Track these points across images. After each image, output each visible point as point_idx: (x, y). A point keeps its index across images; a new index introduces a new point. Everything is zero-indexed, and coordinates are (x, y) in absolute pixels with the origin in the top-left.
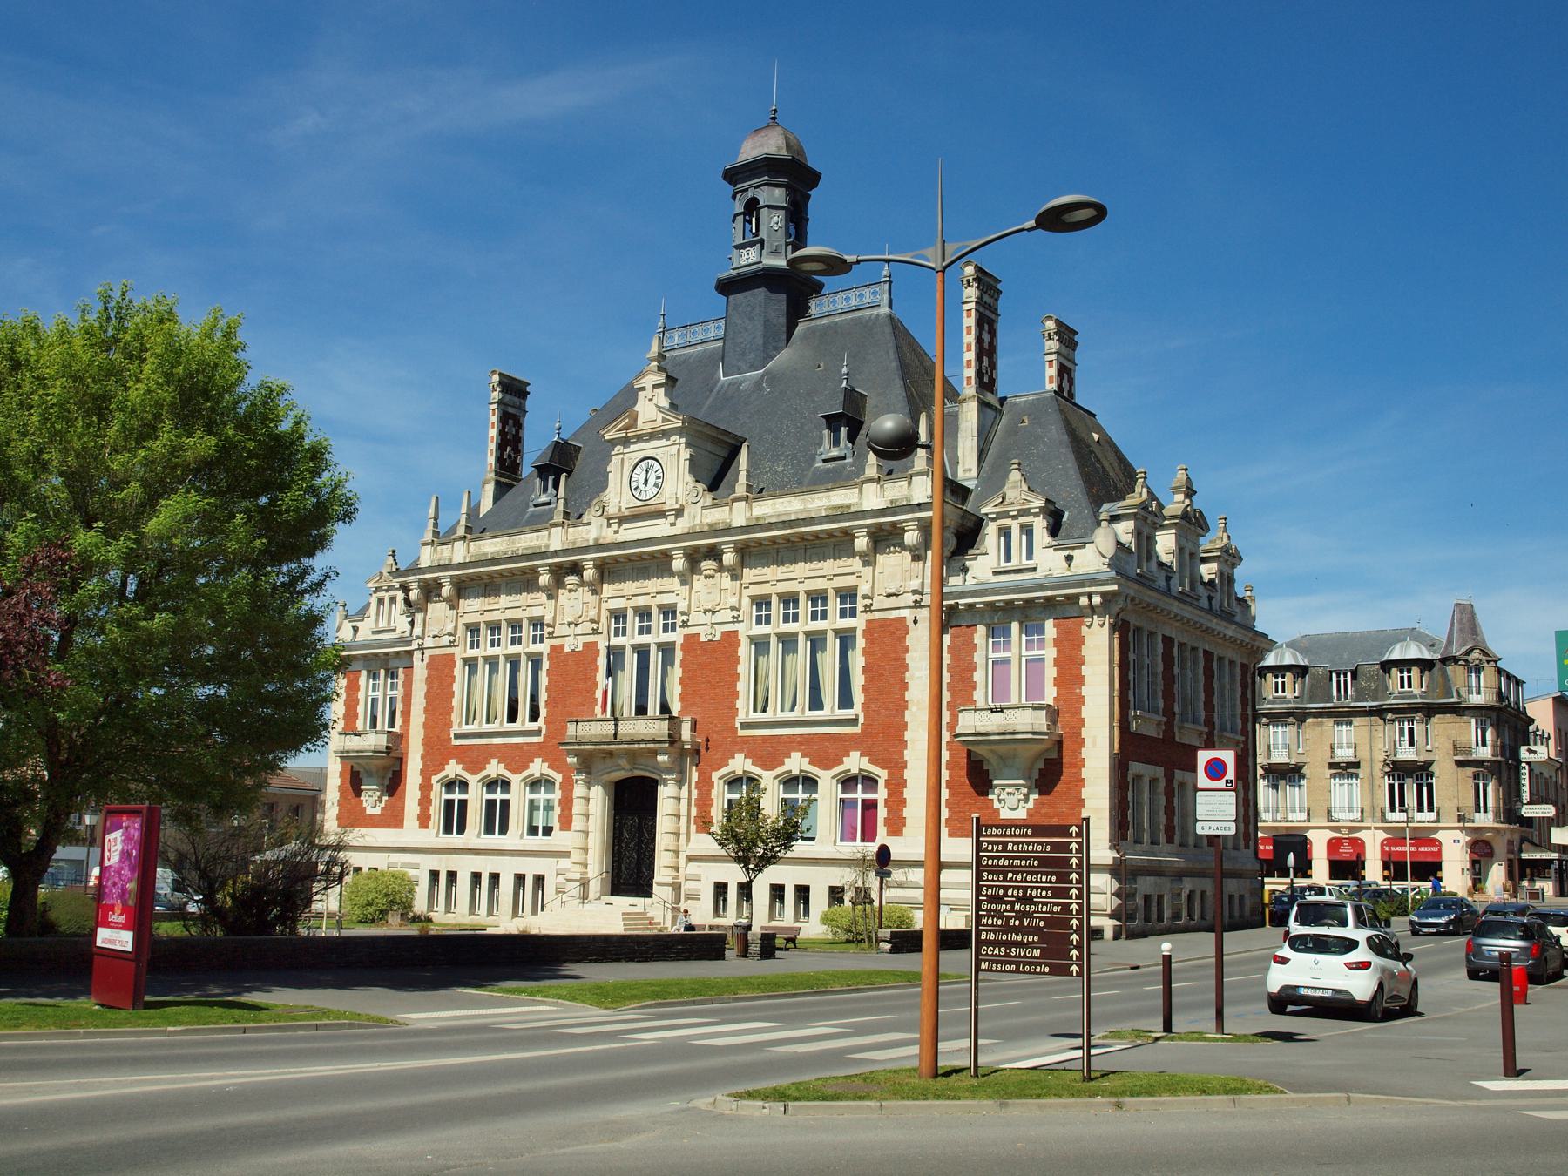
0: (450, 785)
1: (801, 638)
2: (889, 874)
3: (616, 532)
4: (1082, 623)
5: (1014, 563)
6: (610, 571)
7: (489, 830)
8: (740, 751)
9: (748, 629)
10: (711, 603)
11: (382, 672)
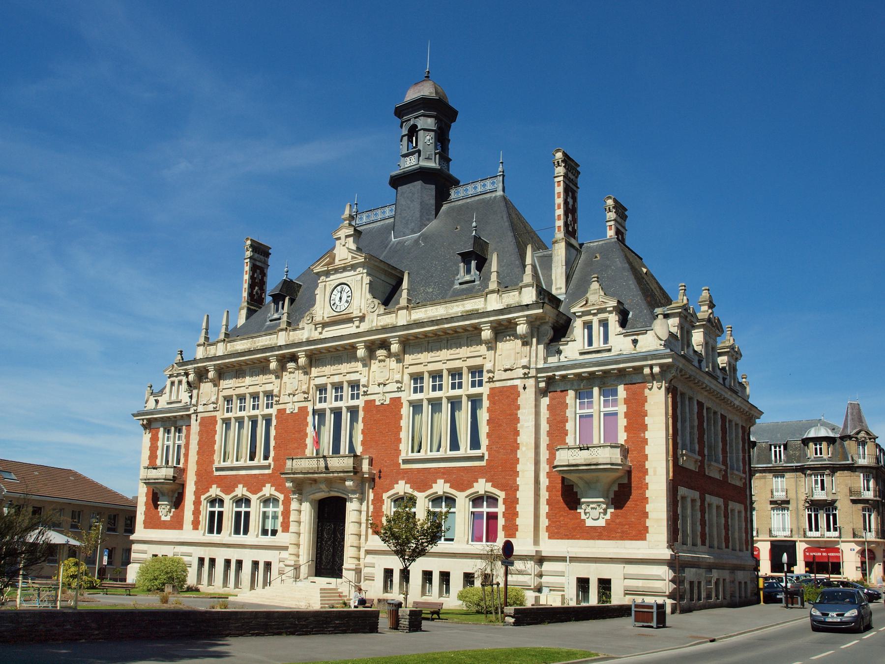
0: (213, 502)
1: (444, 401)
2: (512, 564)
3: (321, 333)
4: (645, 387)
5: (595, 346)
6: (316, 358)
7: (237, 532)
8: (402, 479)
9: (408, 396)
10: (383, 379)
11: (173, 429)
